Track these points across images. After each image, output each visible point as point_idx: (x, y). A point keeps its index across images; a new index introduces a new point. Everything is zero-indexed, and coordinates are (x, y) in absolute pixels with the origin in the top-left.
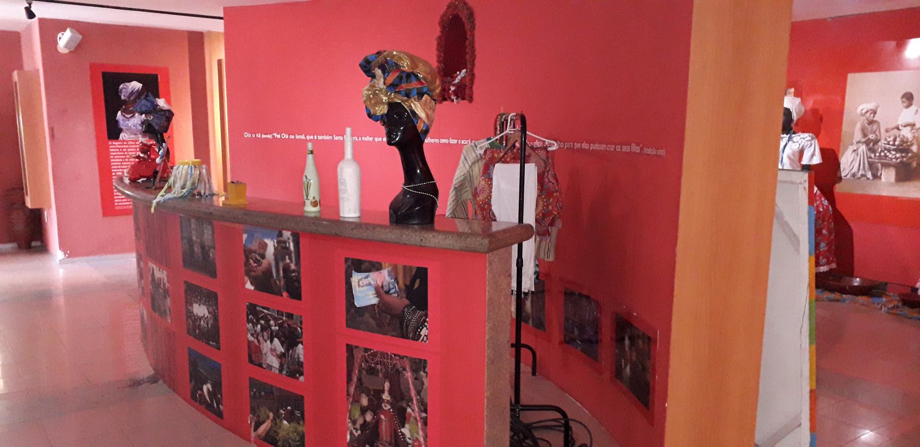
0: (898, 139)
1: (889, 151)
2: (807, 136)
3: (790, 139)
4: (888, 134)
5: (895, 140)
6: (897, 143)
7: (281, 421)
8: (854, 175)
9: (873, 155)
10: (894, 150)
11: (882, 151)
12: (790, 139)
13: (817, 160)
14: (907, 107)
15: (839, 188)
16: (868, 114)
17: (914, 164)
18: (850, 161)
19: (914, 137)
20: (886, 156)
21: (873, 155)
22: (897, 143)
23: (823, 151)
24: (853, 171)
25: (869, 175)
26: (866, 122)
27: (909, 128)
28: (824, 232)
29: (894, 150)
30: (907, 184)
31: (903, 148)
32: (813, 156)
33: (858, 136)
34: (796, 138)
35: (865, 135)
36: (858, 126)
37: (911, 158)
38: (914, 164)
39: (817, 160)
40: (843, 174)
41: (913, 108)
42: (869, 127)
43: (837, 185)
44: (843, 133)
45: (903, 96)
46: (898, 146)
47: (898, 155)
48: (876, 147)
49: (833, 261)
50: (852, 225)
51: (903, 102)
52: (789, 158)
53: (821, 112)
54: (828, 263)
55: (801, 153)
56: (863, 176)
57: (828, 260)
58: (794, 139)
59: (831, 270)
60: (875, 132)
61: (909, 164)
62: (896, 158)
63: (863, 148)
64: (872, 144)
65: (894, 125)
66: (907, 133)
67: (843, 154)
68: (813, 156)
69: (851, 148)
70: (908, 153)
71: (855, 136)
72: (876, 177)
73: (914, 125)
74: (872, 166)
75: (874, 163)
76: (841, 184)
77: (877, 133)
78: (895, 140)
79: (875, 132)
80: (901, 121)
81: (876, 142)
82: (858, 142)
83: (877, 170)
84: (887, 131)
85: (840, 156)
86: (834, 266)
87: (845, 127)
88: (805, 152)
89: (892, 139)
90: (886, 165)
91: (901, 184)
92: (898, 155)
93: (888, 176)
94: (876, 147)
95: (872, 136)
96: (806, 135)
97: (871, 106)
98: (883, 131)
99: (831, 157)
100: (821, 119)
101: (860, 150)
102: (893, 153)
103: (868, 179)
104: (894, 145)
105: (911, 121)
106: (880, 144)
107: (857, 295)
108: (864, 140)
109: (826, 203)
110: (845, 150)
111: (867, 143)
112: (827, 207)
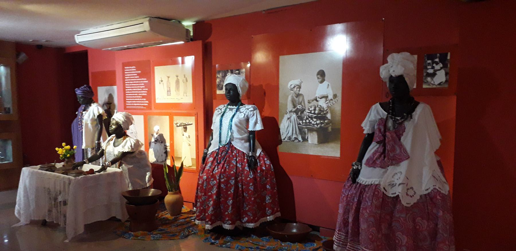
0: (317, 109)
1: (312, 118)
2: (250, 107)
3: (238, 110)
4: (310, 105)
5: (315, 110)
6: (316, 112)
7: (206, 189)
8: (290, 138)
9: (301, 122)
10: (315, 118)
11: (307, 119)
12: (238, 110)
13: (259, 127)
14: (322, 82)
15: (281, 149)
16: (295, 89)
17: (330, 129)
18: (287, 127)
19: (328, 107)
20: (310, 123)
21: (301, 122)
22: (316, 112)
23: (264, 120)
24: (289, 135)
25: (300, 138)
26: (294, 95)
27: (324, 99)
28: (268, 187)
29: (315, 118)
30: (326, 145)
31: (321, 116)
32: (256, 123)
33: (290, 107)
34: (243, 109)
35: (295, 106)
36: (290, 99)
37: (327, 124)
38: (330, 129)
39: (259, 127)
40: (283, 137)
41: (325, 83)
42: (297, 99)
43: (279, 146)
44: (280, 104)
45: (318, 74)
46: (318, 114)
47: (318, 122)
48: (303, 115)
49: (277, 211)
50: (292, 178)
51: (318, 78)
52: (236, 125)
53: (264, 88)
54: (272, 214)
55: (247, 120)
56: (296, 138)
57: (273, 210)
58: (241, 110)
59: (276, 218)
60: (301, 104)
61: (327, 128)
62: (317, 124)
63: (294, 116)
64: (299, 112)
65: (313, 98)
66: (322, 103)
67: (281, 120)
68: (256, 123)
69: (286, 116)
70: (324, 120)
71: (288, 107)
72: (305, 140)
73: (327, 97)
74: (301, 131)
75: (303, 128)
76: (282, 145)
77: (302, 104)
78: (315, 110)
79: (301, 104)
80: (318, 94)
81: (303, 111)
82: (291, 112)
83: (305, 134)
84: (309, 103)
85: (279, 123)
86: (279, 214)
87: (281, 100)
88: (250, 120)
89: (313, 108)
90: (311, 130)
91: (322, 145)
92: (318, 122)
93: (313, 138)
94: (303, 115)
95: (299, 107)
96: (250, 106)
97: (296, 82)
98: (306, 102)
99: (271, 124)
100: (265, 93)
101: (292, 118)
102: (315, 120)
103: (299, 141)
104: (314, 113)
105: (325, 94)
106: (305, 113)
107: (294, 242)
108: (294, 110)
109: (268, 162)
110: (283, 118)
111: (296, 112)
112: (269, 165)
